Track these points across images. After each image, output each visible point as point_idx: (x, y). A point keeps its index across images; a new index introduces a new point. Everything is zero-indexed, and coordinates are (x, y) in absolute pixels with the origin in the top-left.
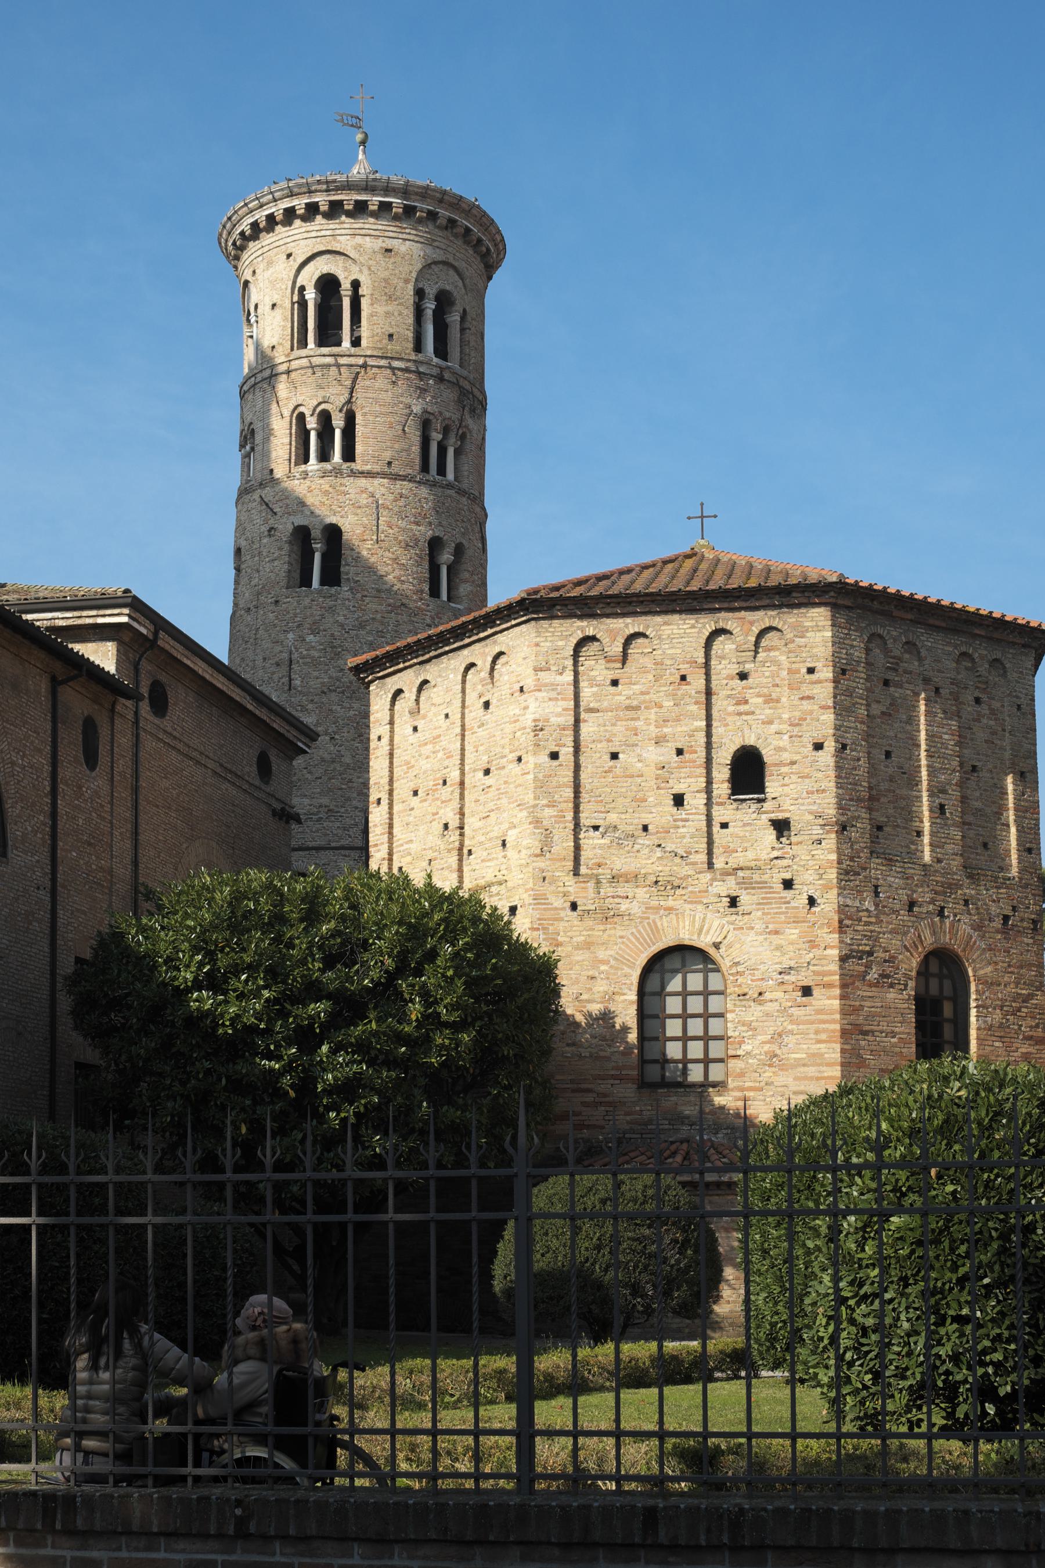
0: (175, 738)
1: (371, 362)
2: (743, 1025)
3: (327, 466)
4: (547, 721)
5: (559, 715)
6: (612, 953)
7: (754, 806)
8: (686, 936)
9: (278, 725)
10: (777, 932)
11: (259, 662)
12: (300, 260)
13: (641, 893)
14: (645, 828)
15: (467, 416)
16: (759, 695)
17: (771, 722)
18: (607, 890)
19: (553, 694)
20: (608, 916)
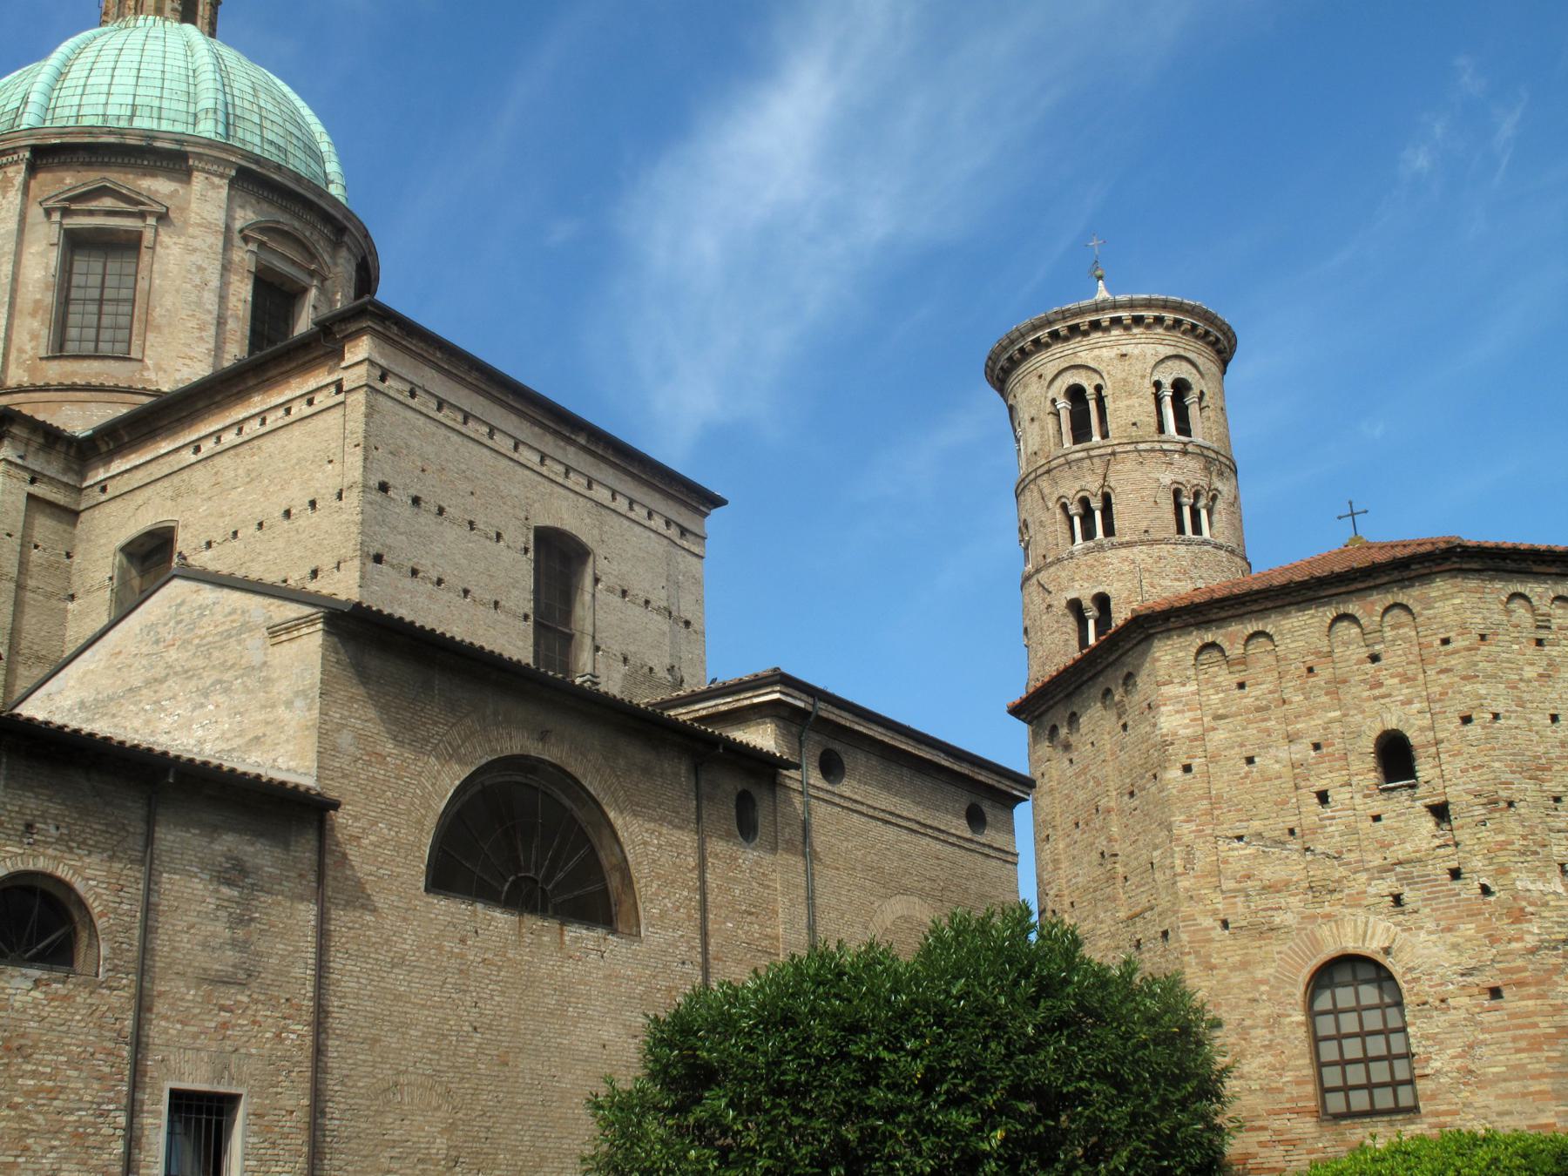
0: (856, 801)
1: (1118, 449)
2: (1428, 1039)
3: (1091, 544)
4: (1175, 734)
5: (1186, 727)
6: (1272, 971)
7: (1405, 793)
8: (1351, 946)
9: (983, 777)
10: (1449, 930)
12: (1049, 378)
13: (1294, 901)
14: (1292, 832)
15: (1215, 479)
16: (1392, 676)
17: (1410, 702)
18: (1258, 902)
19: (1180, 707)
20: (1265, 930)
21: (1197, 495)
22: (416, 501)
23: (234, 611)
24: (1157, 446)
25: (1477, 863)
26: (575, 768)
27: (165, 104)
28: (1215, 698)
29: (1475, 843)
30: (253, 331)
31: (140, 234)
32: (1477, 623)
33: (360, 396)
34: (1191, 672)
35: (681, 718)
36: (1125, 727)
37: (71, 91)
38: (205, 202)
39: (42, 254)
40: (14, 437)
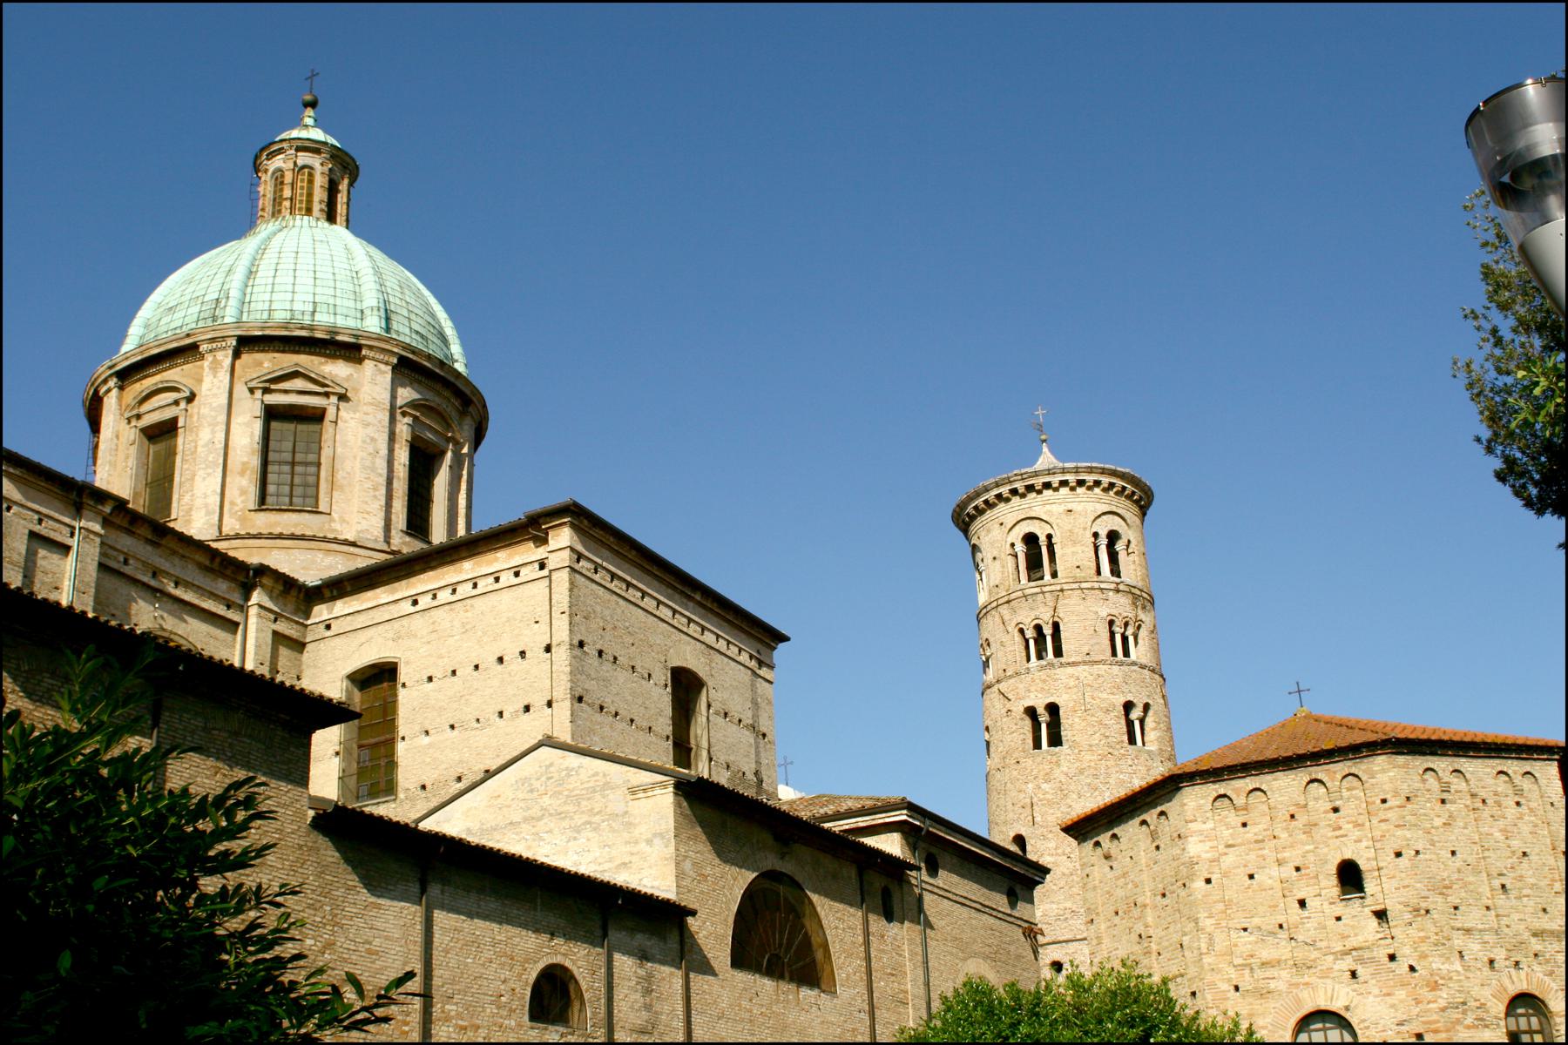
3: (1043, 662)
11: (1010, 806)
13: (1284, 974)
14: (1281, 926)
18: (1259, 974)
21: (1126, 624)
22: (600, 653)
23: (596, 774)
24: (1096, 585)
25: (1407, 950)
26: (799, 878)
27: (339, 302)
28: (1227, 833)
29: (1405, 937)
30: (410, 489)
31: (324, 410)
32: (1405, 790)
33: (565, 574)
34: (1209, 814)
35: (837, 829)
36: (1158, 848)
37: (262, 289)
38: (371, 384)
39: (247, 425)
40: (262, 586)
